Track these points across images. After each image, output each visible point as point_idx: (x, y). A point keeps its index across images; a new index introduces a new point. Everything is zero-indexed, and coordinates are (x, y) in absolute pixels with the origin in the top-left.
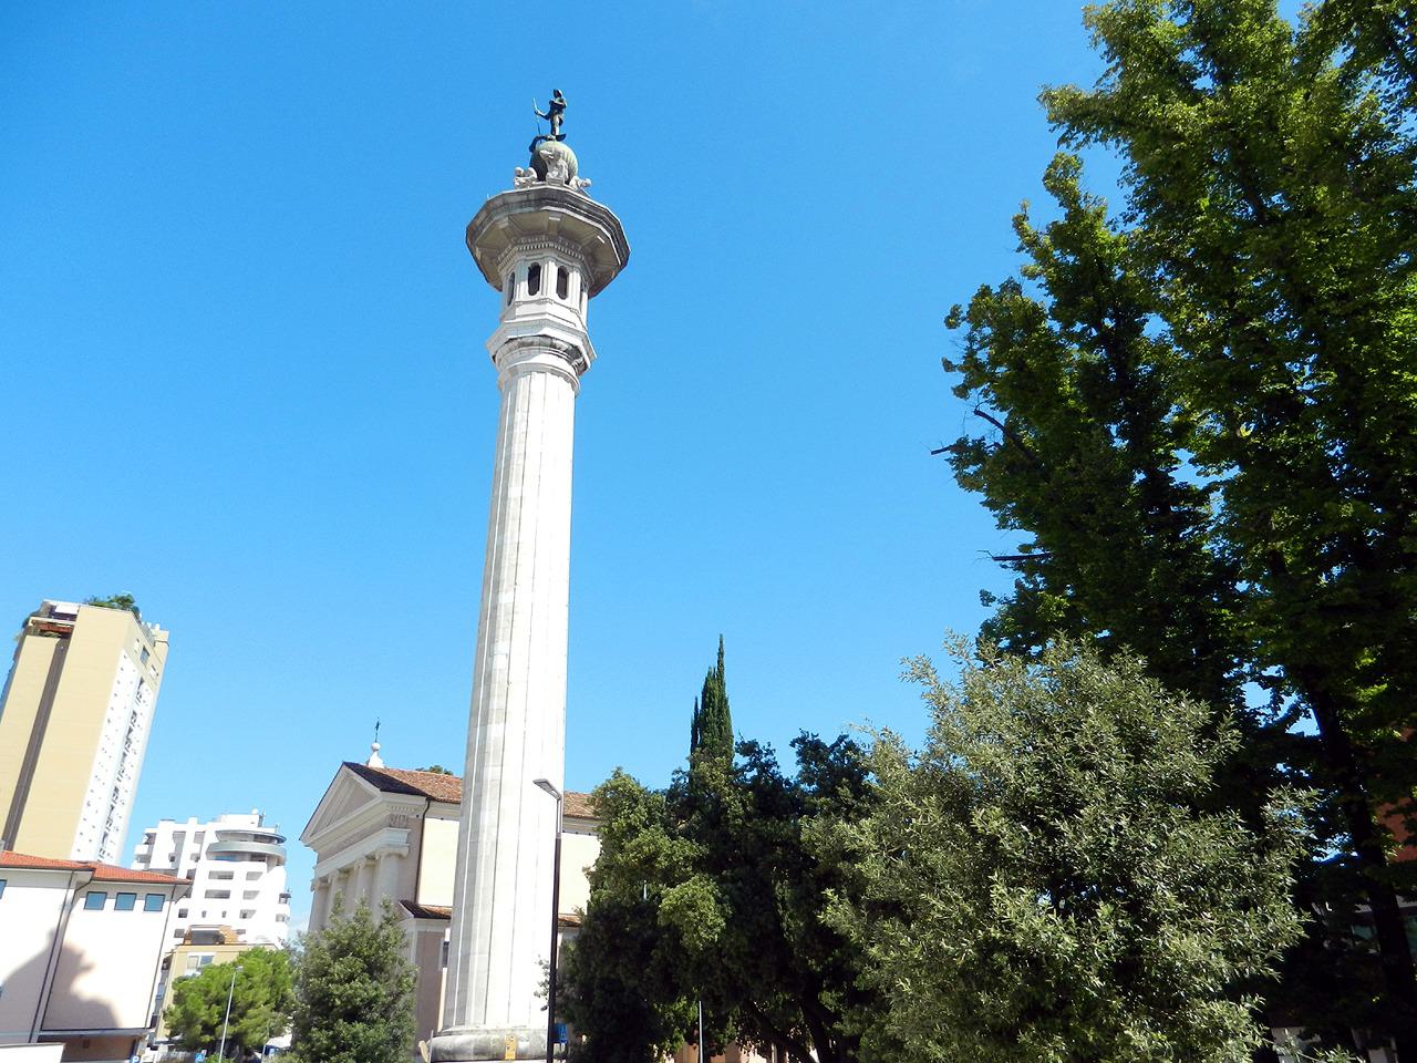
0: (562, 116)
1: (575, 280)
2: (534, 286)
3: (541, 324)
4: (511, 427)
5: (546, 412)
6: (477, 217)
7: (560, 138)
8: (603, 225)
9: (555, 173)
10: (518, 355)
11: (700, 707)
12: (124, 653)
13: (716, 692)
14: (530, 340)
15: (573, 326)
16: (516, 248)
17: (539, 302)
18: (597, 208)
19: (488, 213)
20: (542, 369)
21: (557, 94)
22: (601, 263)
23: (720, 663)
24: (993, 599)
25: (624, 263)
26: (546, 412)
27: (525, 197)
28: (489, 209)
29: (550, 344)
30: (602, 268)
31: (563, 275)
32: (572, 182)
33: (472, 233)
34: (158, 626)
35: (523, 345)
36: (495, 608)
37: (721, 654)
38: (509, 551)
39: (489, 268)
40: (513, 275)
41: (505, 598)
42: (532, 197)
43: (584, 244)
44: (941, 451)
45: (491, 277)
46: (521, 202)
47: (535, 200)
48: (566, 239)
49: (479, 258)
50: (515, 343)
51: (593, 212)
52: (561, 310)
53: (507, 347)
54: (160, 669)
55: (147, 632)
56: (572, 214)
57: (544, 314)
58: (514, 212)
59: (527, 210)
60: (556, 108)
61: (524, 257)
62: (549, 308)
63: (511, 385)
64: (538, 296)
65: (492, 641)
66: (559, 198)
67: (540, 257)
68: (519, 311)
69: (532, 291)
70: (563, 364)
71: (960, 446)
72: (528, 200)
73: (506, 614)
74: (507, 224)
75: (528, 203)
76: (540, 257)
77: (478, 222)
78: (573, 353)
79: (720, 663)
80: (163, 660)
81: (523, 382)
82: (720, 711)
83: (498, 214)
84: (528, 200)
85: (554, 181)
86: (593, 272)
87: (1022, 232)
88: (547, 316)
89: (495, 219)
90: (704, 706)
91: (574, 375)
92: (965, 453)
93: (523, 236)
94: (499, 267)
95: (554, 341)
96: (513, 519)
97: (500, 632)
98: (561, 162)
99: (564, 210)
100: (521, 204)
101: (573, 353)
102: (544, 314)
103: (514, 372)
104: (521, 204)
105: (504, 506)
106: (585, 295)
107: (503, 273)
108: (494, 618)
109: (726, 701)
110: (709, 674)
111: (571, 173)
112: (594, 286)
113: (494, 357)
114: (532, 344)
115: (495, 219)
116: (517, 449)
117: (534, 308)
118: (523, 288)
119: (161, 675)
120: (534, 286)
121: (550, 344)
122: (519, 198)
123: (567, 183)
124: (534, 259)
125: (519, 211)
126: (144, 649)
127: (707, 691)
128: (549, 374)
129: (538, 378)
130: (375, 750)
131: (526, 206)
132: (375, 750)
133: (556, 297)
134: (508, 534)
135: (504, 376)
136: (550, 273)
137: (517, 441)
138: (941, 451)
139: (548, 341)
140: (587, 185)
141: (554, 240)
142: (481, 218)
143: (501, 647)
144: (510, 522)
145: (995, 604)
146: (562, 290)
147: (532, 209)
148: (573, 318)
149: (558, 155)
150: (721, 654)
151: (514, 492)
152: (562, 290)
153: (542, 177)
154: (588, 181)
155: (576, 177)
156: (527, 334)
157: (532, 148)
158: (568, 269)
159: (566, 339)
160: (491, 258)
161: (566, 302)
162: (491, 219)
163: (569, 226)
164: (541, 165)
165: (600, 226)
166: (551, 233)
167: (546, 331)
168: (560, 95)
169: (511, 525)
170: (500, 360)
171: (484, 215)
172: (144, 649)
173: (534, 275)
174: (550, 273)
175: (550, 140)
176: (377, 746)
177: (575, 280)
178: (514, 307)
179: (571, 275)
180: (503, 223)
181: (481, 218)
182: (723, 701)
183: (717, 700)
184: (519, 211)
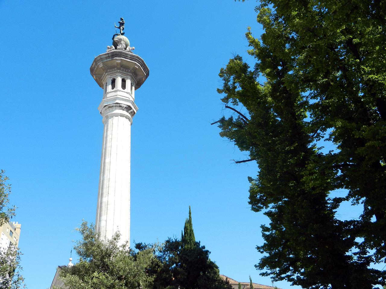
0: (124, 27)
1: (128, 82)
2: (113, 86)
3: (115, 99)
4: (106, 137)
5: (119, 132)
6: (92, 65)
7: (123, 34)
8: (137, 62)
9: (120, 46)
10: (108, 111)
11: (183, 234)
12: (2, 233)
13: (189, 228)
14: (112, 105)
15: (128, 99)
16: (107, 74)
17: (115, 91)
18: (133, 56)
19: (96, 63)
20: (117, 115)
21: (122, 19)
22: (139, 77)
23: (190, 217)
24: (253, 180)
25: (148, 75)
26: (119, 132)
27: (107, 55)
28: (96, 61)
29: (120, 106)
30: (139, 77)
31: (124, 81)
32: (128, 49)
33: (92, 70)
34: (17, 223)
35: (110, 107)
36: (101, 203)
37: (190, 213)
38: (106, 182)
39: (100, 83)
40: (107, 83)
41: (105, 200)
42: (110, 55)
43: (131, 69)
44: (215, 123)
45: (101, 85)
46: (106, 57)
47: (111, 56)
48: (124, 68)
49: (95, 79)
50: (107, 107)
51: (132, 58)
52: (124, 93)
53: (104, 109)
54: (18, 238)
55: (12, 225)
56: (124, 59)
57: (117, 95)
58: (104, 61)
59: (108, 60)
60: (122, 24)
61: (110, 76)
62: (118, 93)
63: (107, 122)
64: (115, 89)
65: (100, 216)
66: (119, 54)
67: (126, 77)
68: (108, 95)
69: (113, 88)
70: (125, 113)
71: (222, 121)
72: (109, 56)
73: (105, 205)
74: (102, 66)
75: (109, 57)
76: (126, 77)
77: (93, 66)
78: (128, 108)
79: (190, 217)
80: (19, 234)
81: (110, 120)
82: (190, 235)
83: (99, 63)
84: (109, 56)
85: (119, 49)
86: (136, 79)
87: (249, 38)
88: (118, 96)
89: (98, 64)
90: (185, 234)
91: (130, 116)
92: (224, 123)
93: (109, 69)
94: (102, 81)
95: (121, 105)
96: (107, 170)
97: (103, 212)
98: (122, 42)
99: (121, 58)
100: (106, 58)
101: (128, 108)
102: (117, 95)
103: (107, 117)
104: (106, 58)
105: (104, 166)
106: (133, 88)
107: (104, 83)
108: (101, 207)
109: (193, 231)
110: (186, 221)
111: (127, 46)
112: (138, 84)
113: (101, 113)
114: (113, 107)
115: (98, 64)
116: (108, 145)
117: (113, 94)
118: (110, 87)
119: (18, 240)
120: (113, 86)
121: (120, 106)
122: (105, 56)
123: (125, 49)
124: (113, 76)
125: (106, 60)
126: (11, 231)
127: (186, 228)
128: (119, 117)
129: (115, 118)
130: (70, 261)
131: (108, 58)
132: (70, 261)
133: (121, 89)
134: (105, 176)
135: (104, 119)
136: (119, 81)
137: (108, 142)
138: (215, 123)
139: (118, 105)
140: (133, 49)
141: (119, 69)
142: (94, 65)
143: (103, 218)
144: (106, 171)
145: (254, 182)
146: (124, 86)
147: (110, 59)
148: (128, 95)
149: (121, 40)
150: (190, 213)
151: (107, 160)
152: (124, 86)
153: (116, 48)
154: (134, 48)
155: (129, 47)
156: (111, 103)
157: (113, 38)
158: (126, 79)
159: (125, 103)
160: (99, 78)
161: (125, 90)
162: (97, 64)
163: (124, 63)
164: (115, 44)
165: (135, 62)
166: (118, 67)
167: (118, 101)
168: (122, 19)
169: (106, 172)
170: (103, 113)
171: (94, 63)
172: (11, 231)
173: (113, 82)
174: (119, 81)
175: (119, 35)
176: (71, 259)
177: (128, 82)
178: (107, 94)
179: (127, 81)
180: (101, 65)
181: (94, 65)
182: (191, 231)
183: (189, 232)
184: (106, 60)
